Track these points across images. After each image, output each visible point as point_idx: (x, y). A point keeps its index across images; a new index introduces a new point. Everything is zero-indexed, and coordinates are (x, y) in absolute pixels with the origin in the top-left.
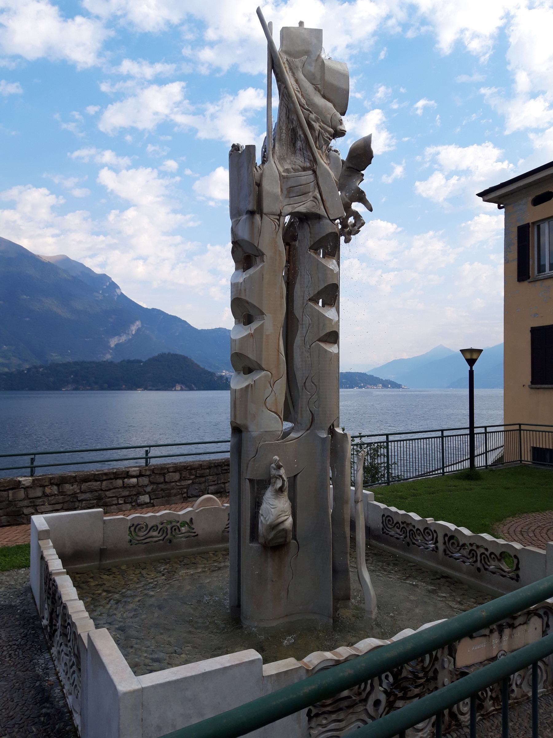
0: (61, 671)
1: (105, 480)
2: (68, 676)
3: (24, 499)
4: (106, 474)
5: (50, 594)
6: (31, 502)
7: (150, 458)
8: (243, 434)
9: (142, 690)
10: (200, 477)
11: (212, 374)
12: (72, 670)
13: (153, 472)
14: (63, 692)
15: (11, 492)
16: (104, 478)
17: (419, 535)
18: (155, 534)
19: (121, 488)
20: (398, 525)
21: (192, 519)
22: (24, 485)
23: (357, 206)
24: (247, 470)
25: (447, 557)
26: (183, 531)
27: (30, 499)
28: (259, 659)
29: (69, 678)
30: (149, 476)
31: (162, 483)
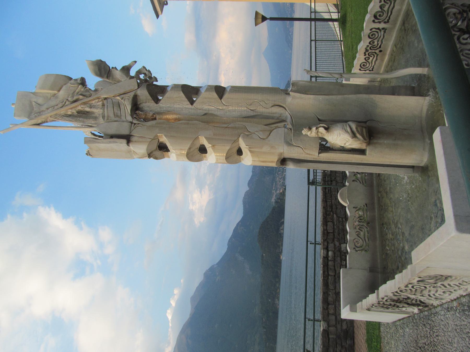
0: (450, 297)
1: (328, 272)
2: (452, 291)
3: (336, 327)
4: (324, 272)
5: (395, 305)
6: (339, 323)
7: (315, 241)
8: (286, 157)
9: (456, 216)
10: (332, 209)
11: (274, 209)
12: (448, 286)
13: (326, 240)
14: (465, 296)
15: (331, 336)
16: (326, 273)
17: (374, 42)
18: (362, 233)
19: (334, 262)
20: (367, 59)
21: (354, 207)
22: (326, 327)
23: (133, 73)
24: (312, 155)
25: (390, 21)
26: (362, 214)
27: (336, 324)
28: (440, 129)
29: (455, 290)
30: (328, 243)
31: (334, 235)
